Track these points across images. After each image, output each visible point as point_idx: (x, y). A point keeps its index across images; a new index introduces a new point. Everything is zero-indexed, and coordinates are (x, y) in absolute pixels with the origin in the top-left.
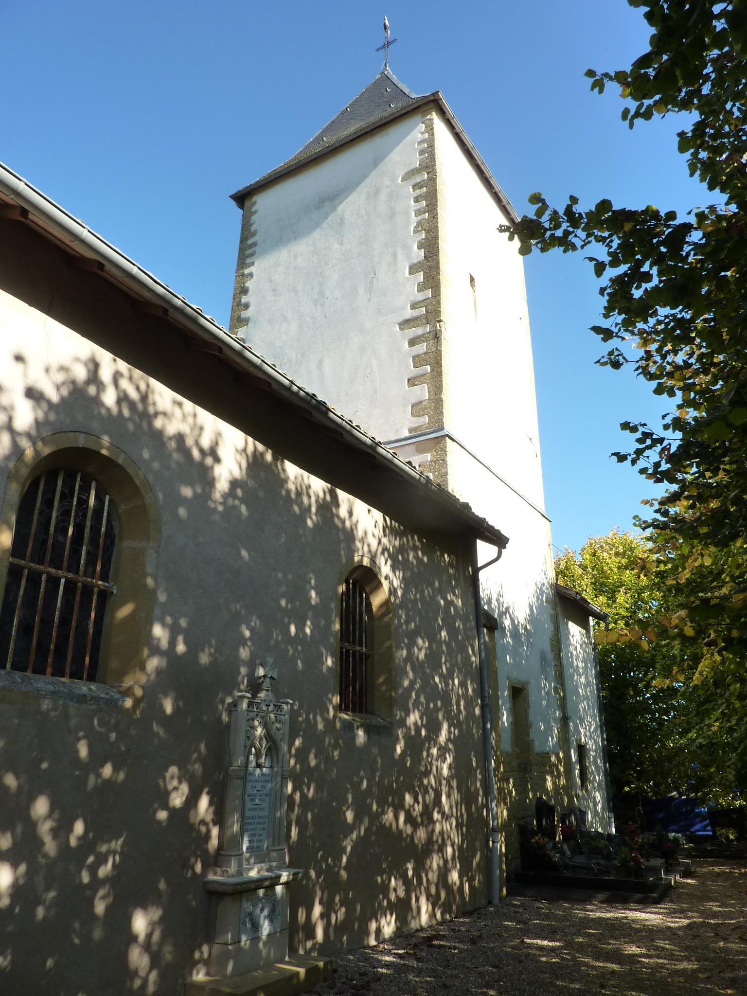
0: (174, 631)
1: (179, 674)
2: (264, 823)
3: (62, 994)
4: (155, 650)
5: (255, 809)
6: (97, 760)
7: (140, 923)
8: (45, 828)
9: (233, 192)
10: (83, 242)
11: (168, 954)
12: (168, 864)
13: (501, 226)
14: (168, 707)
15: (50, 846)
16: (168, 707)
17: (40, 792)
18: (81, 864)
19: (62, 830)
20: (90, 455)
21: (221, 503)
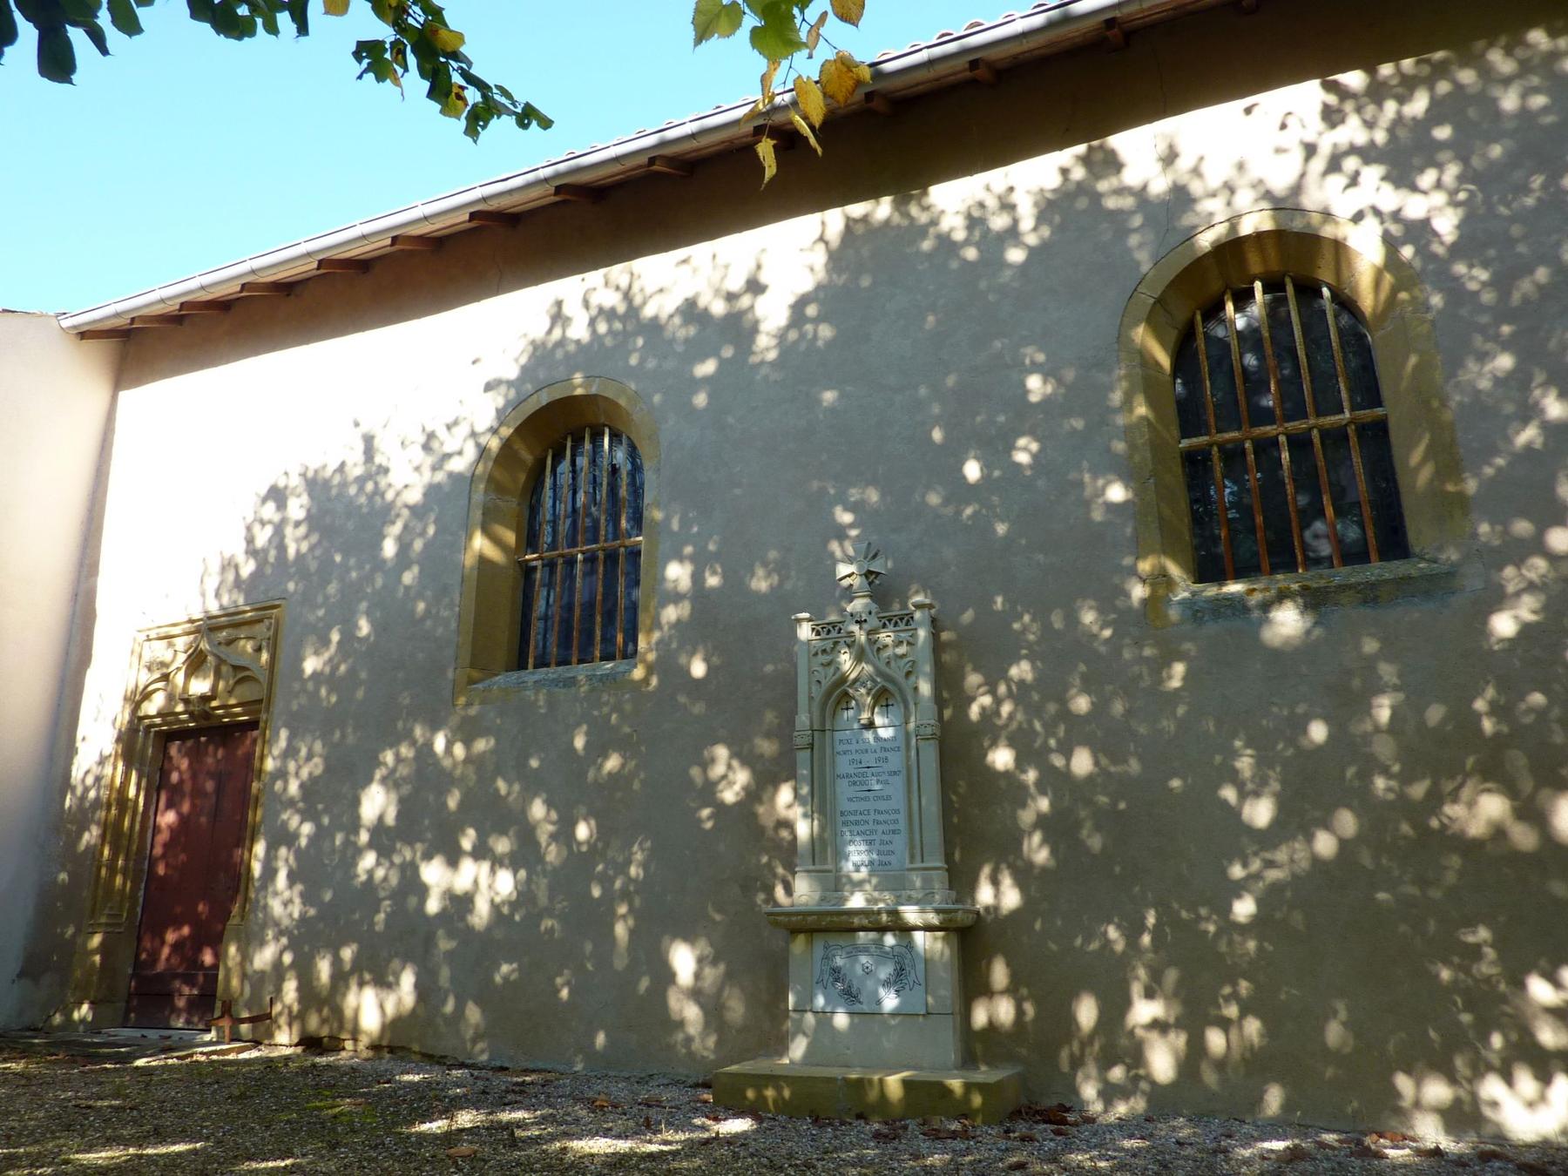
0: (700, 567)
1: (709, 619)
2: (896, 821)
3: (1558, 888)
4: (676, 597)
5: (865, 799)
6: (598, 749)
7: (683, 960)
8: (544, 832)
9: (690, 33)
10: (617, 159)
11: (736, 1008)
12: (724, 878)
13: (466, 133)
14: (698, 669)
15: (552, 854)
16: (698, 669)
17: (535, 795)
18: (591, 877)
19: (564, 833)
20: (567, 406)
21: (1431, 89)
